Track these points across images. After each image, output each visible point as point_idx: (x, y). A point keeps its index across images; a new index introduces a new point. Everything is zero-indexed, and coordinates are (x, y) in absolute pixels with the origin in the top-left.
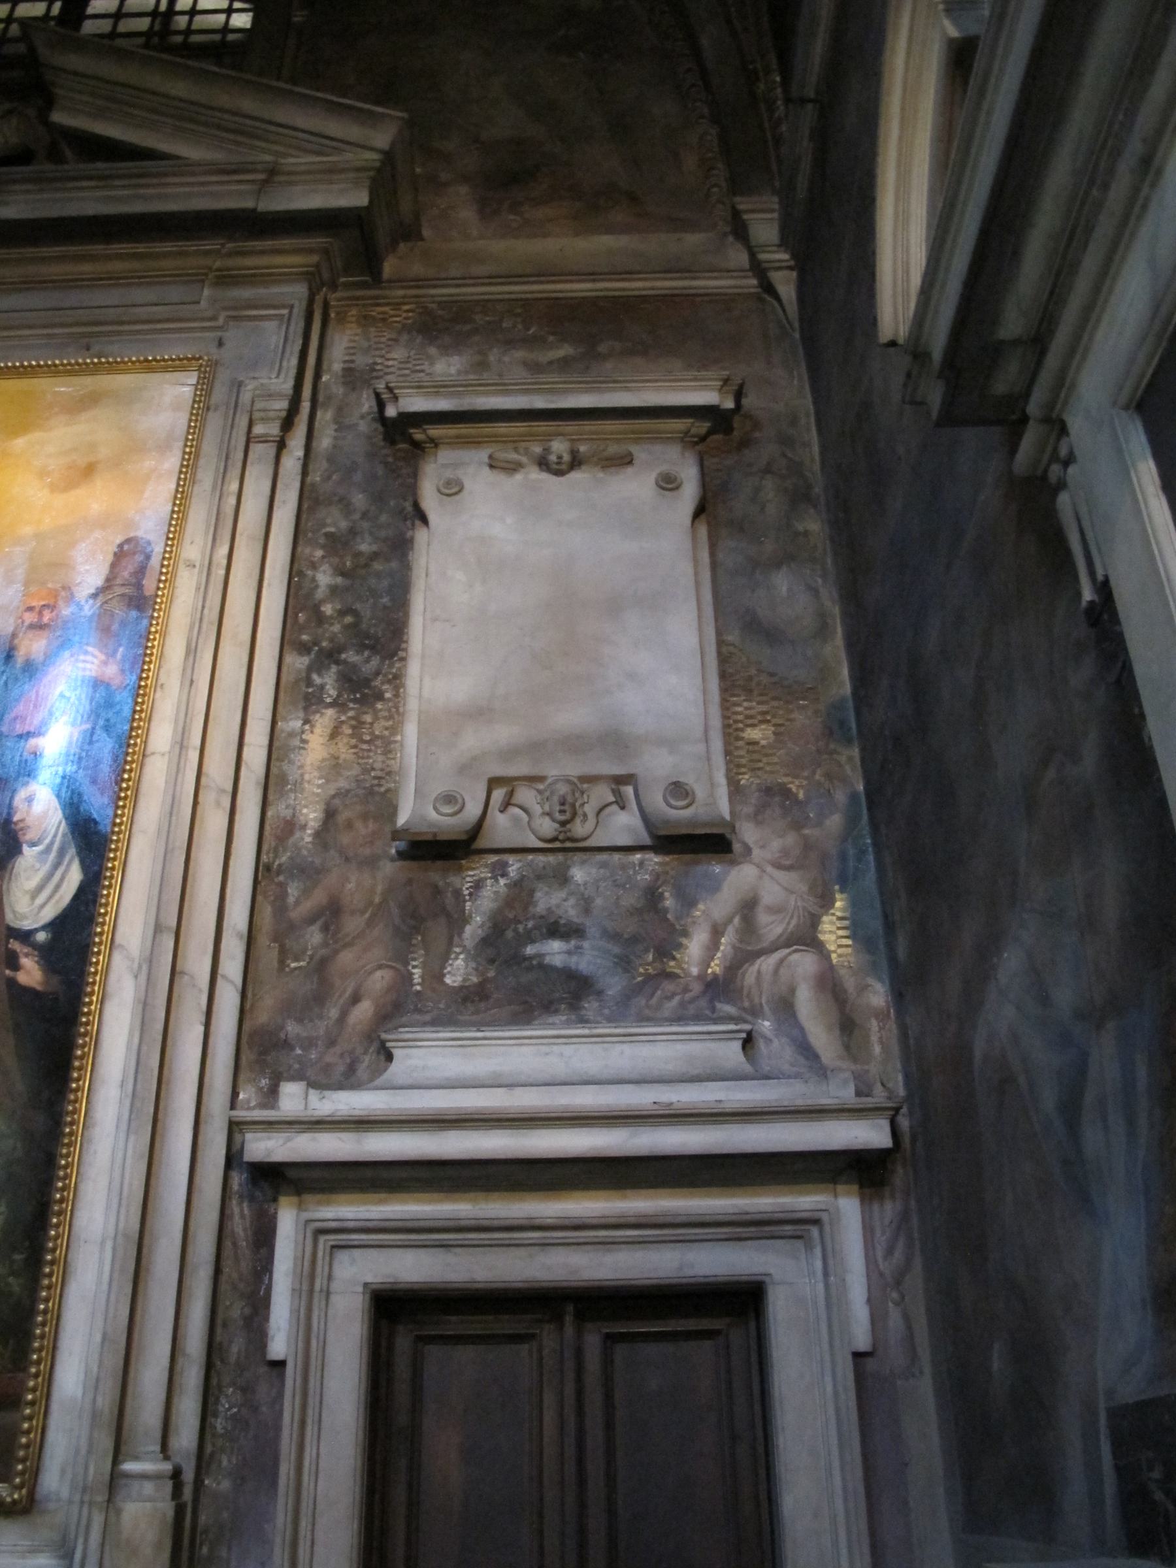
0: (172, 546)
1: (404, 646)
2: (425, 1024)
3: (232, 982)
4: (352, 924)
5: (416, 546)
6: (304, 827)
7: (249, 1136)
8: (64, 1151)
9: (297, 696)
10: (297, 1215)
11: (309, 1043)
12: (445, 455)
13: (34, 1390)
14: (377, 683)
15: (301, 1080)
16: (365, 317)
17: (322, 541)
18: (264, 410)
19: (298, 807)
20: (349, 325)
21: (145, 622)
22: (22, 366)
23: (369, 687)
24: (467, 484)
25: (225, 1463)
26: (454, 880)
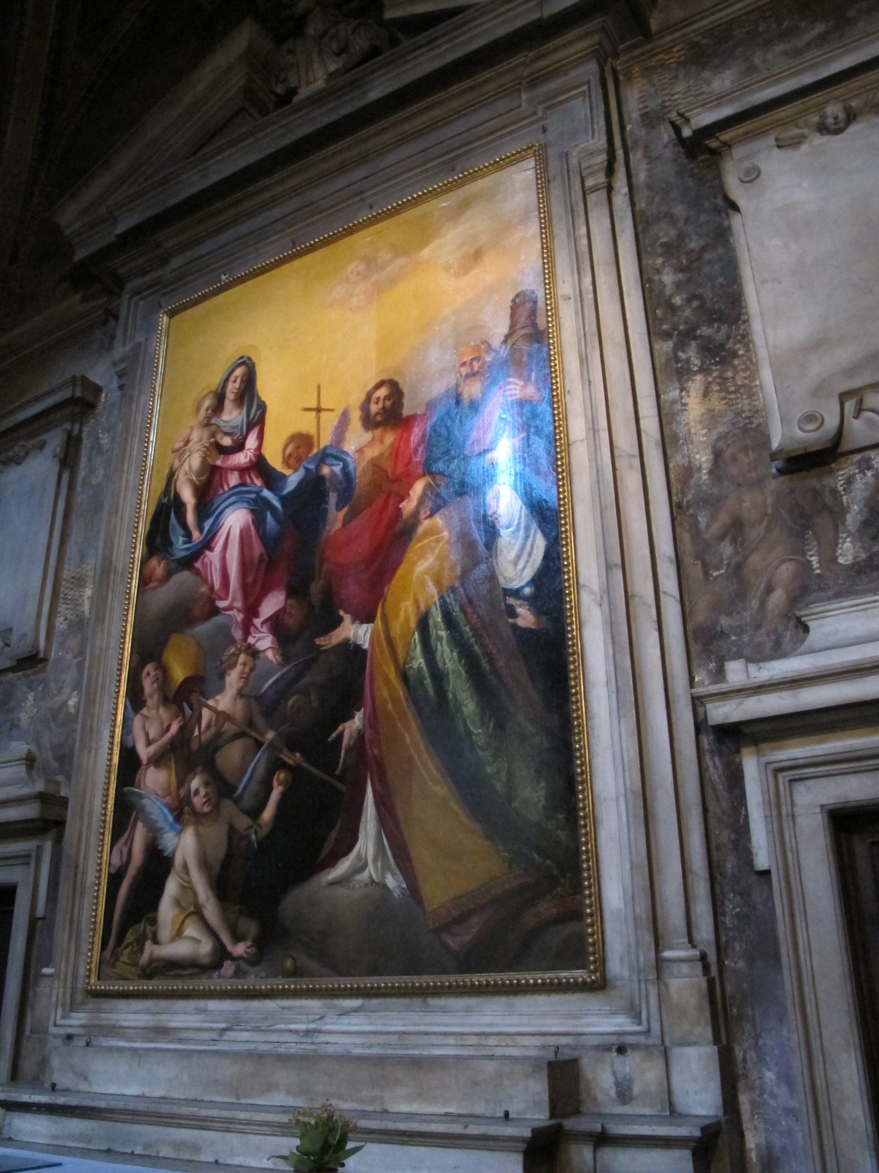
0: (550, 289)
1: (744, 311)
2: (829, 598)
3: (671, 596)
4: (754, 533)
5: (734, 230)
6: (699, 469)
7: (708, 706)
8: (577, 738)
9: (669, 372)
10: (758, 761)
11: (740, 631)
12: (738, 152)
13: (590, 906)
14: (730, 345)
15: (740, 658)
16: (646, 69)
17: (660, 250)
18: (589, 167)
19: (692, 455)
20: (635, 81)
21: (545, 349)
22: (414, 198)
23: (724, 349)
24: (763, 167)
25: (737, 948)
26: (828, 481)
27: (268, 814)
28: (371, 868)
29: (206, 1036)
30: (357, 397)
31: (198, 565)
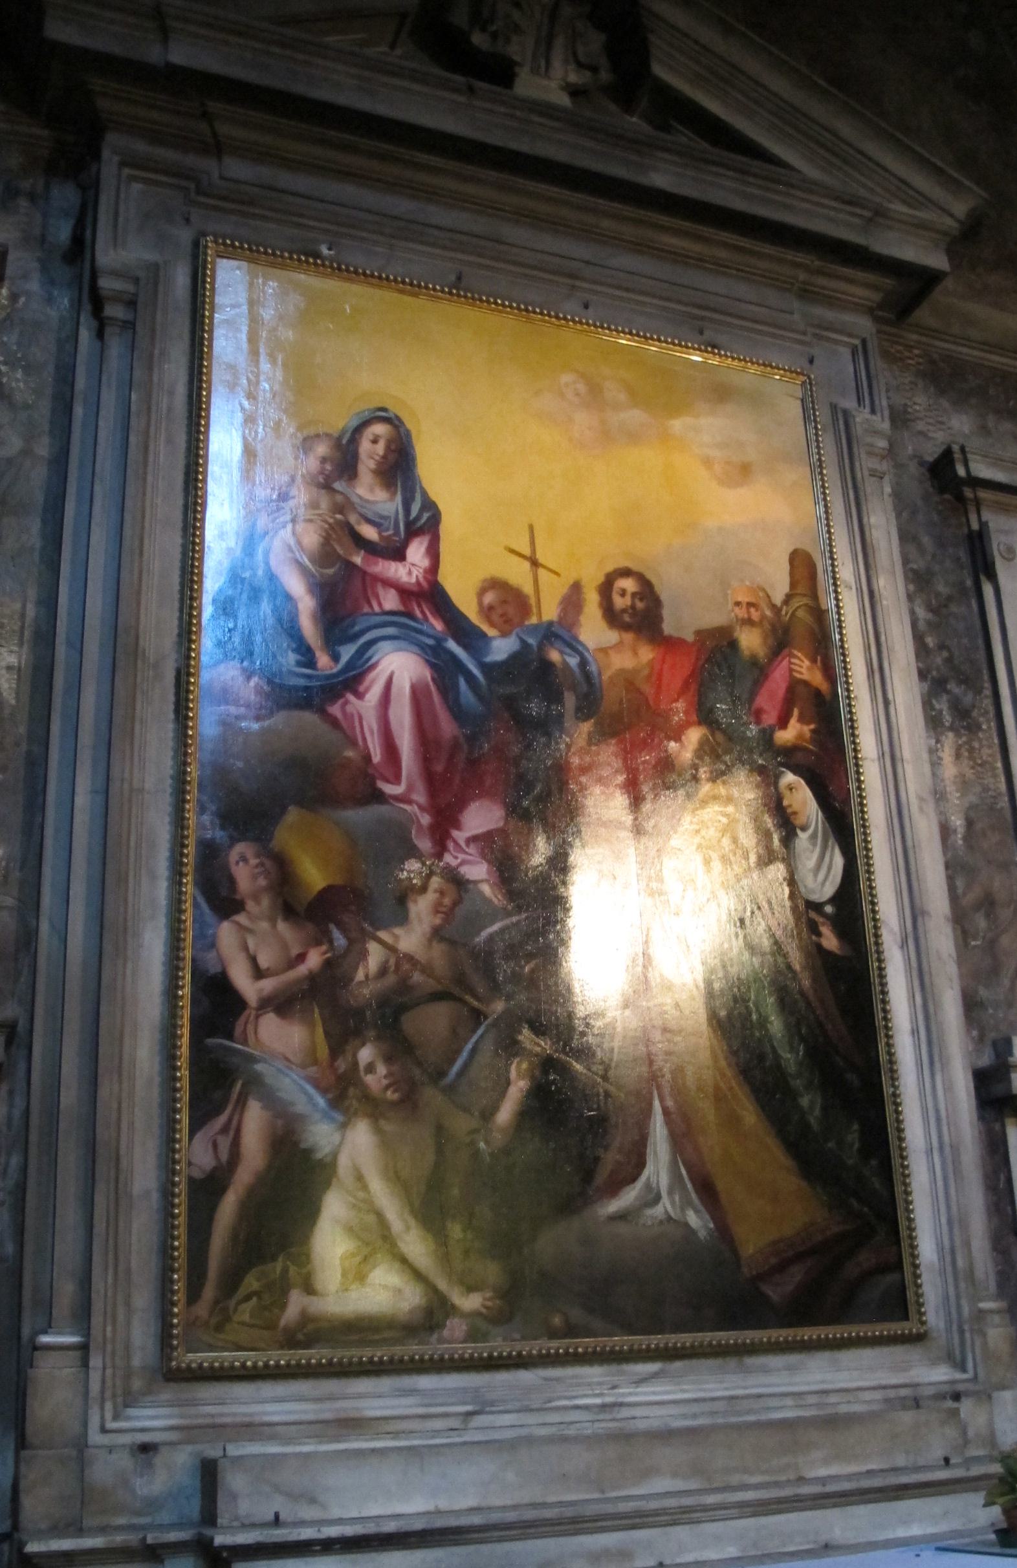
27: (505, 1114)
28: (665, 1200)
29: (439, 1424)
30: (591, 579)
31: (335, 710)
